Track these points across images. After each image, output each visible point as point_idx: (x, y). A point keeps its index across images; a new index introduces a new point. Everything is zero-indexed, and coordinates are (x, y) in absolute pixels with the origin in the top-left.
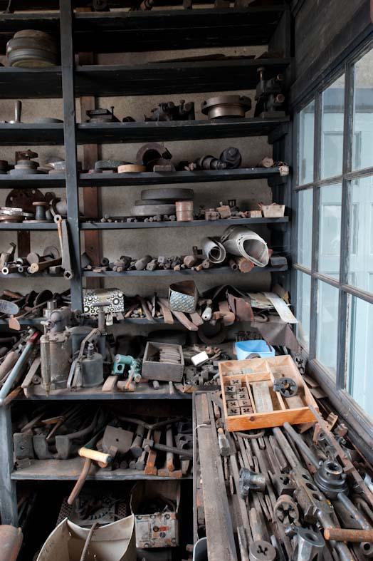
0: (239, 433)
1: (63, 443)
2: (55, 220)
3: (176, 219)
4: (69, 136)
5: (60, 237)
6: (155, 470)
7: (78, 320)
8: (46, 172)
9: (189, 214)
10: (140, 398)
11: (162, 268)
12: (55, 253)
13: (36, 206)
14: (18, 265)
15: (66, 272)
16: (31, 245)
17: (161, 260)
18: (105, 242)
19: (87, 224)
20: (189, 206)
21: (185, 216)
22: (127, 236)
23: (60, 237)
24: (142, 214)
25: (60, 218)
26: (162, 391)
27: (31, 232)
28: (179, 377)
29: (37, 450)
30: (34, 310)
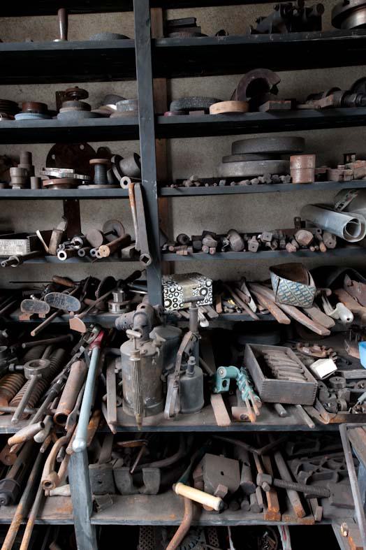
1: (152, 477)
2: (122, 184)
3: (291, 180)
4: (143, 62)
5: (133, 208)
6: (280, 514)
7: (161, 319)
8: (107, 116)
9: (311, 172)
11: (268, 248)
12: (119, 229)
13: (94, 164)
14: (77, 247)
15: (142, 256)
16: (81, 218)
17: (266, 237)
18: (176, 212)
19: (168, 188)
20: (311, 161)
21: (303, 176)
22: (202, 204)
23: (133, 208)
24: (239, 174)
25: (128, 180)
27: (81, 201)
29: (119, 485)
30: (97, 302)
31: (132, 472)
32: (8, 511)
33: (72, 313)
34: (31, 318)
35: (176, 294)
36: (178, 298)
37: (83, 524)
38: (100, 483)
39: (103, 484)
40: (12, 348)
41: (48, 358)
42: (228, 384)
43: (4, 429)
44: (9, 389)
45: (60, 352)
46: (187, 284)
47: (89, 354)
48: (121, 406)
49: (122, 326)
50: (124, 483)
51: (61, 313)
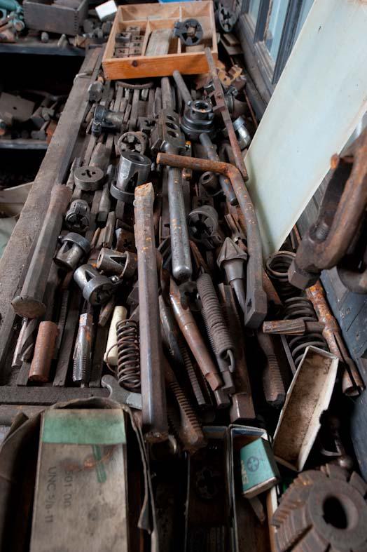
0: (120, 83)
10: (24, 52)
26: (51, 45)
28: (72, 28)
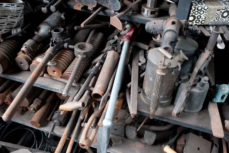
7: (185, 33)
31: (137, 130)
32: (59, 129)
33: (113, 12)
34: (82, 8)
35: (202, 12)
36: (202, 16)
37: (102, 150)
38: (116, 130)
39: (117, 131)
40: (67, 28)
41: (91, 42)
42: (225, 98)
43: (58, 90)
44: (63, 63)
45: (100, 35)
46: (214, 5)
47: (121, 43)
48: (140, 92)
49: (151, 30)
50: (131, 135)
51: (104, 9)
